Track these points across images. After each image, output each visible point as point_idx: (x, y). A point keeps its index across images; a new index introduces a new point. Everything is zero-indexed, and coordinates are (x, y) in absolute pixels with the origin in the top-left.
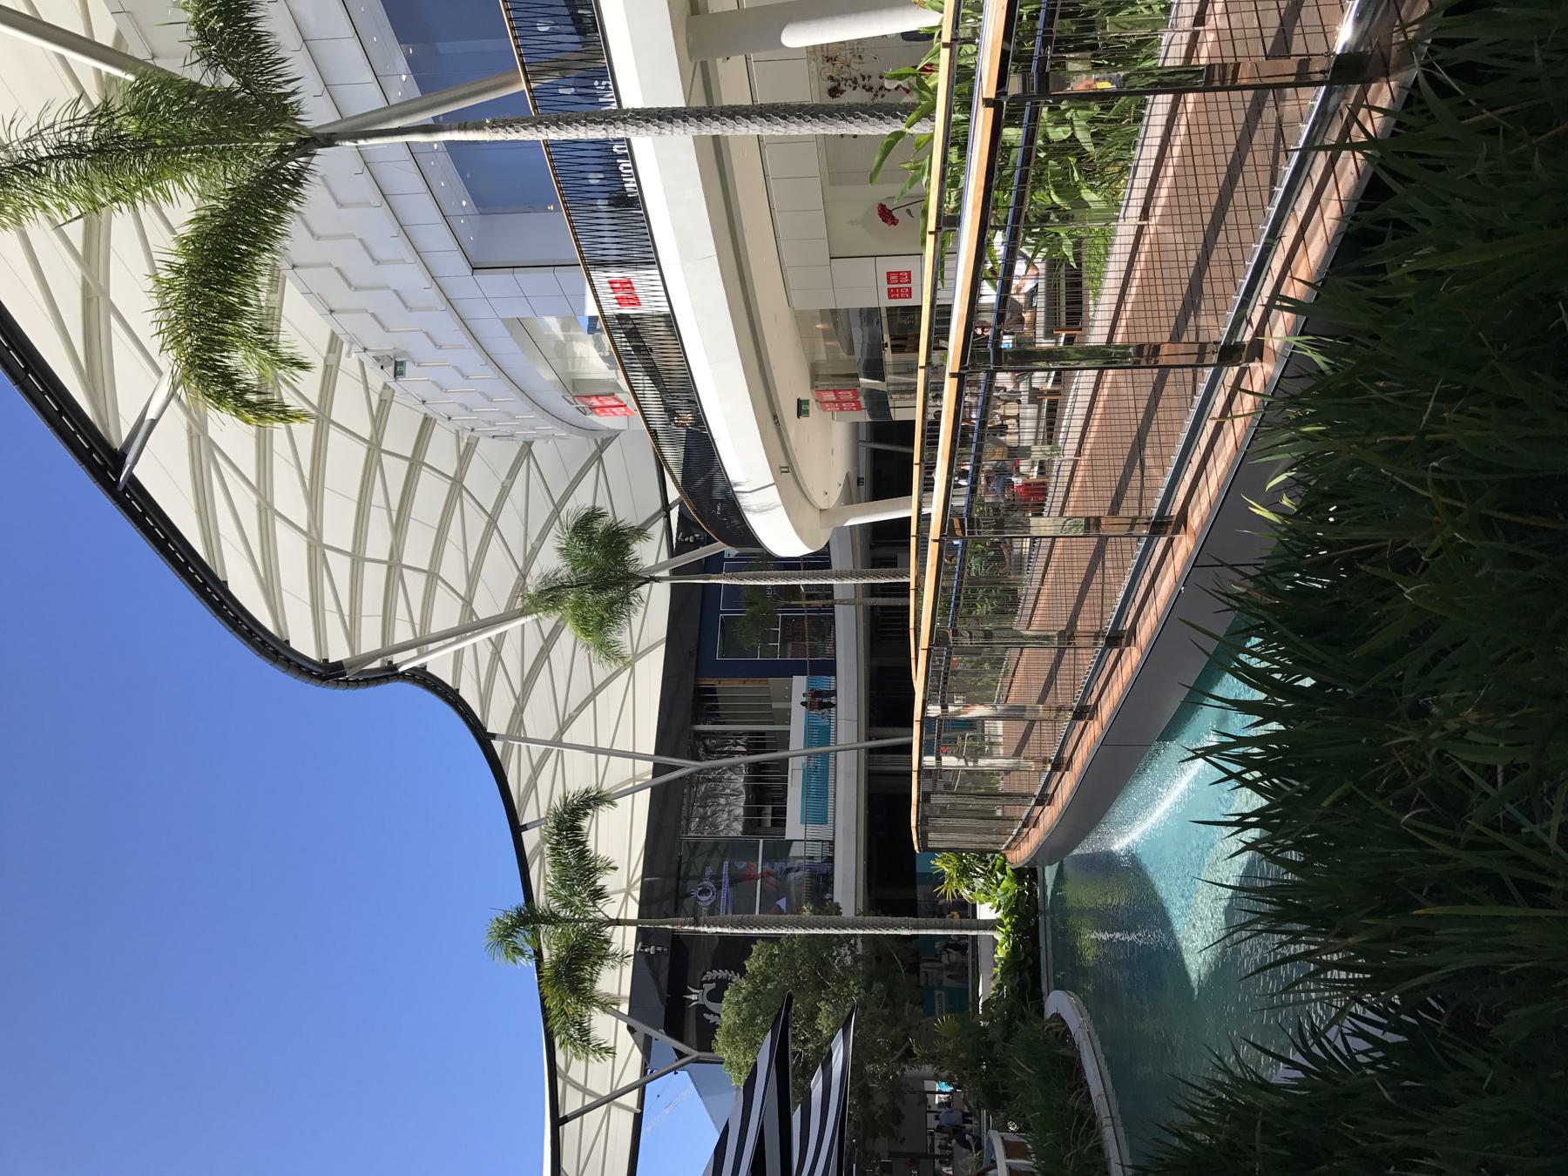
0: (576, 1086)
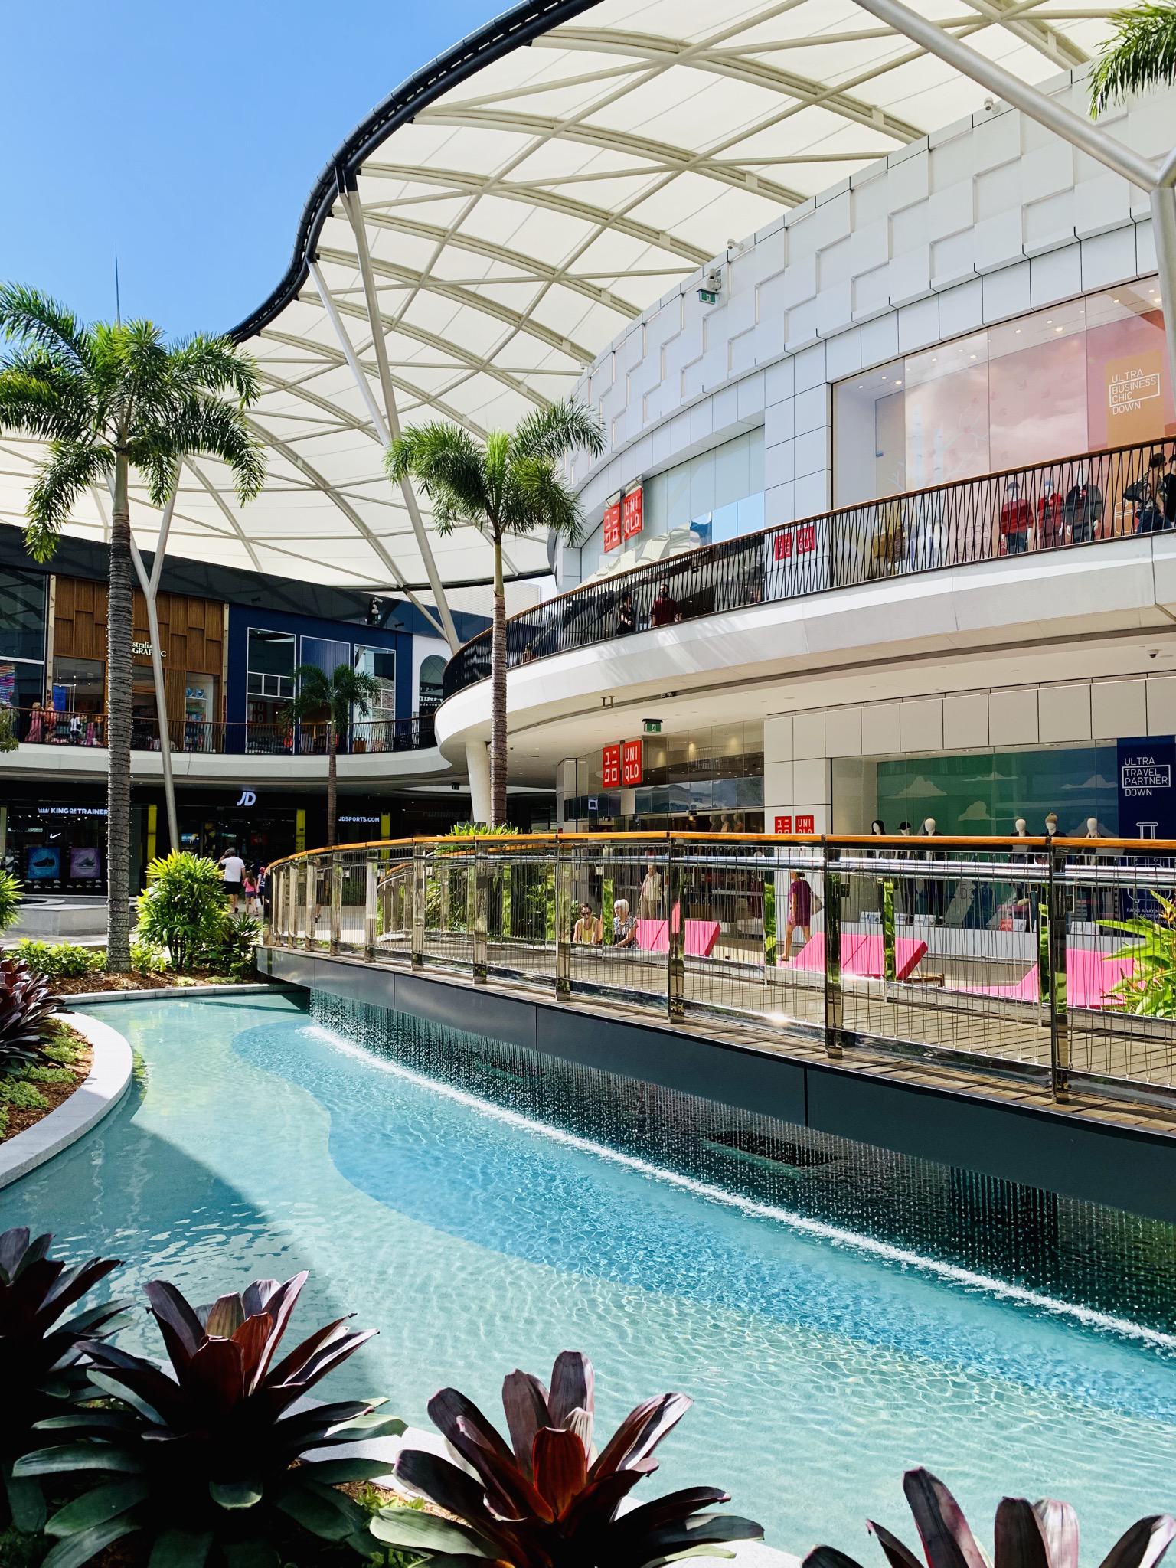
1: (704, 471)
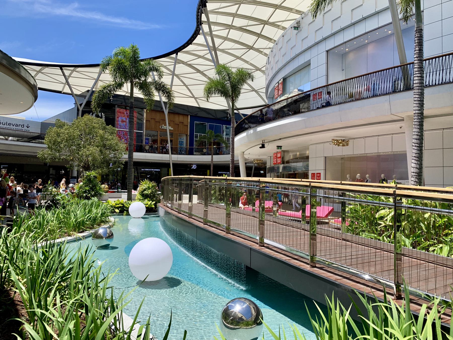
0: (71, 74)
1: (298, 76)
